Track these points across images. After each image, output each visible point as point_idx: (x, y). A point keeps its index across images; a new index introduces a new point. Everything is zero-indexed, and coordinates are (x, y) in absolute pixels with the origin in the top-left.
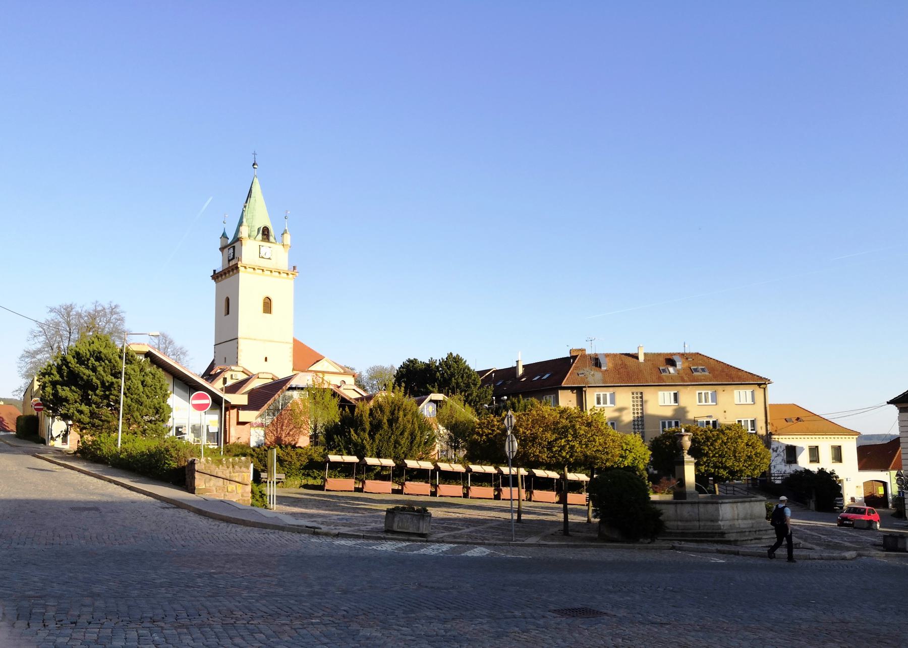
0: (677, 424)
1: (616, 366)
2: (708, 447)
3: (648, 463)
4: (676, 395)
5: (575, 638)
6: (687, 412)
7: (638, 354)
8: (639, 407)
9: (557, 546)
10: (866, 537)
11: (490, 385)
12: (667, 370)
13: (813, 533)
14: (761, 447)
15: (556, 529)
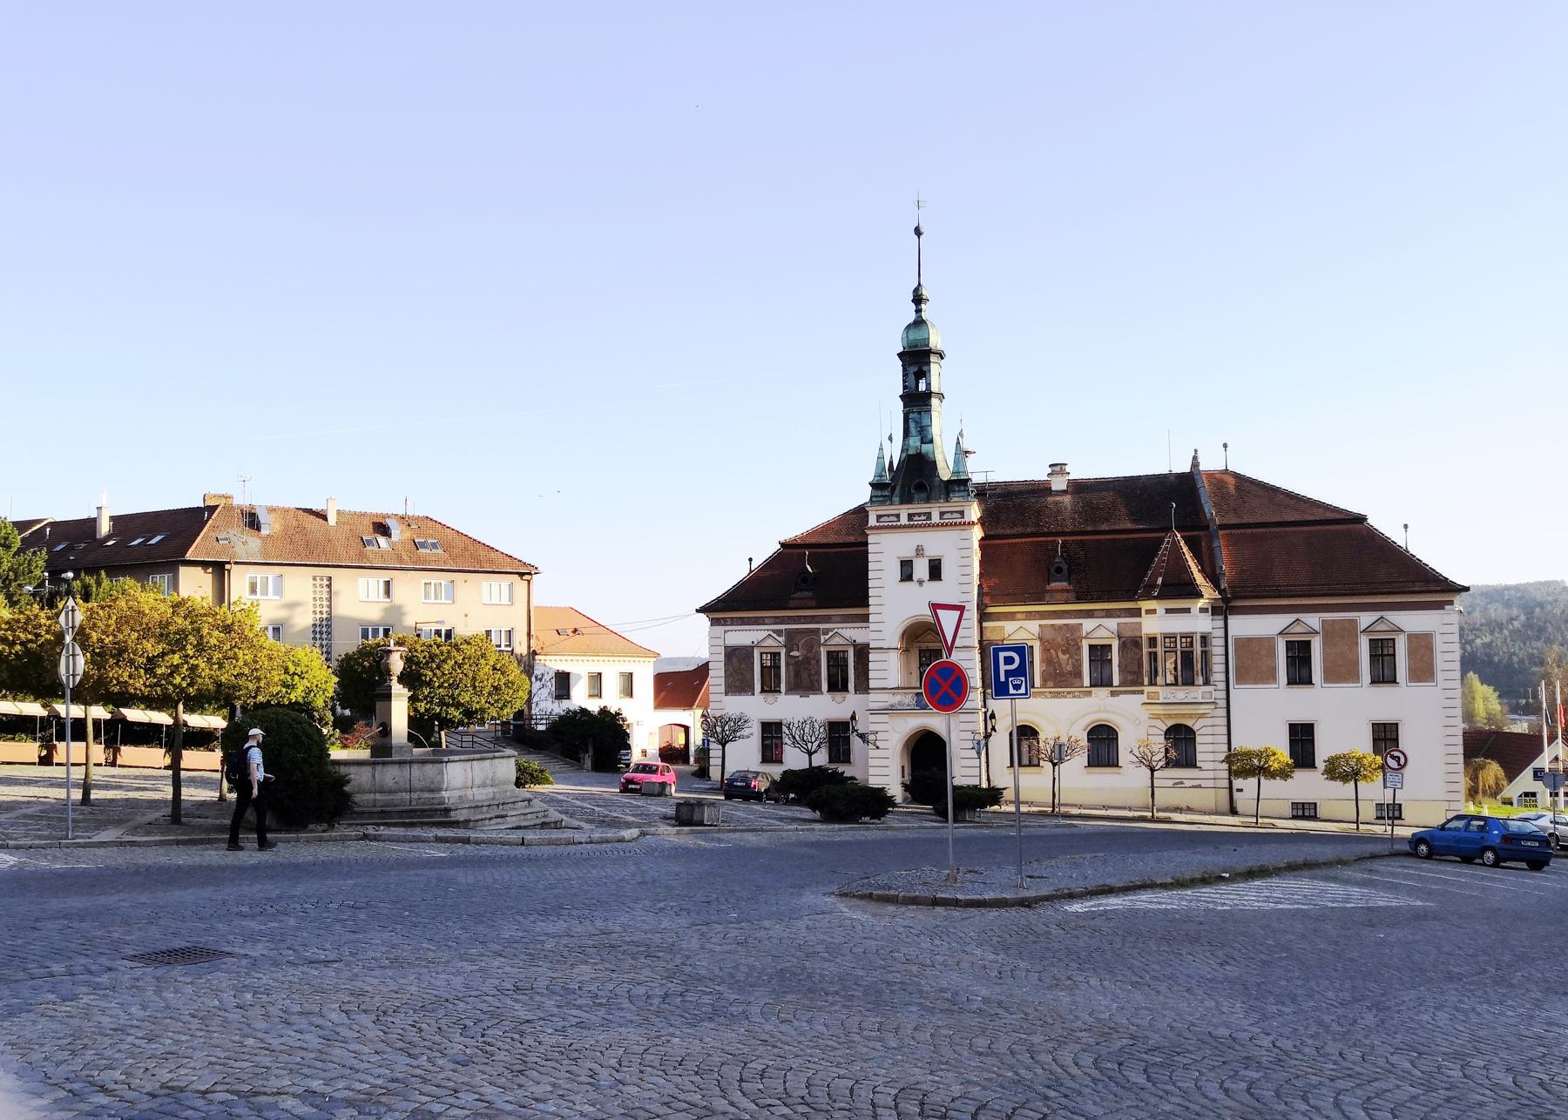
0: (386, 632)
1: (286, 528)
2: (432, 671)
3: (332, 697)
4: (387, 584)
5: (165, 1000)
6: (403, 614)
7: (326, 510)
8: (325, 603)
9: (157, 843)
10: (656, 807)
11: (40, 551)
12: (374, 541)
13: (585, 805)
14: (515, 672)
15: (158, 814)
